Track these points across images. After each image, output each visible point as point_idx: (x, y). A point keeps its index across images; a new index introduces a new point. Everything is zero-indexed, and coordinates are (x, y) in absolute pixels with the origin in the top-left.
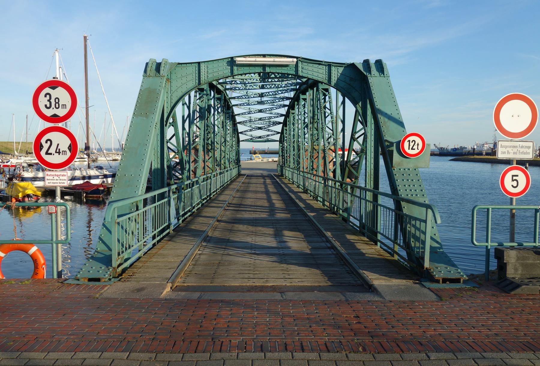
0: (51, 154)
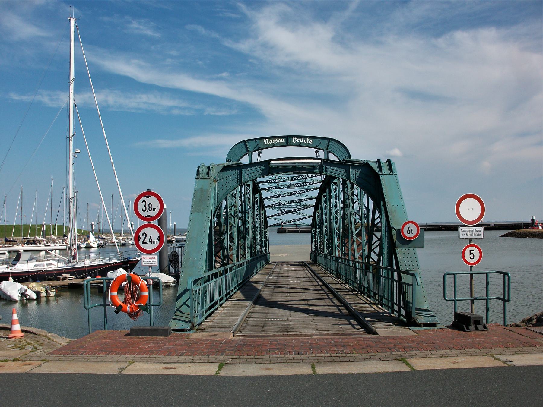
0: (146, 243)
